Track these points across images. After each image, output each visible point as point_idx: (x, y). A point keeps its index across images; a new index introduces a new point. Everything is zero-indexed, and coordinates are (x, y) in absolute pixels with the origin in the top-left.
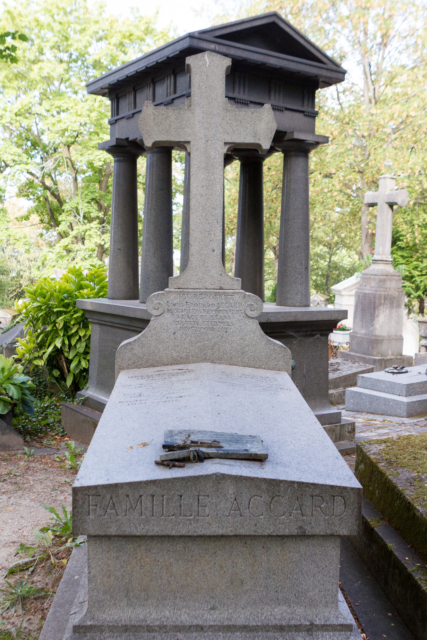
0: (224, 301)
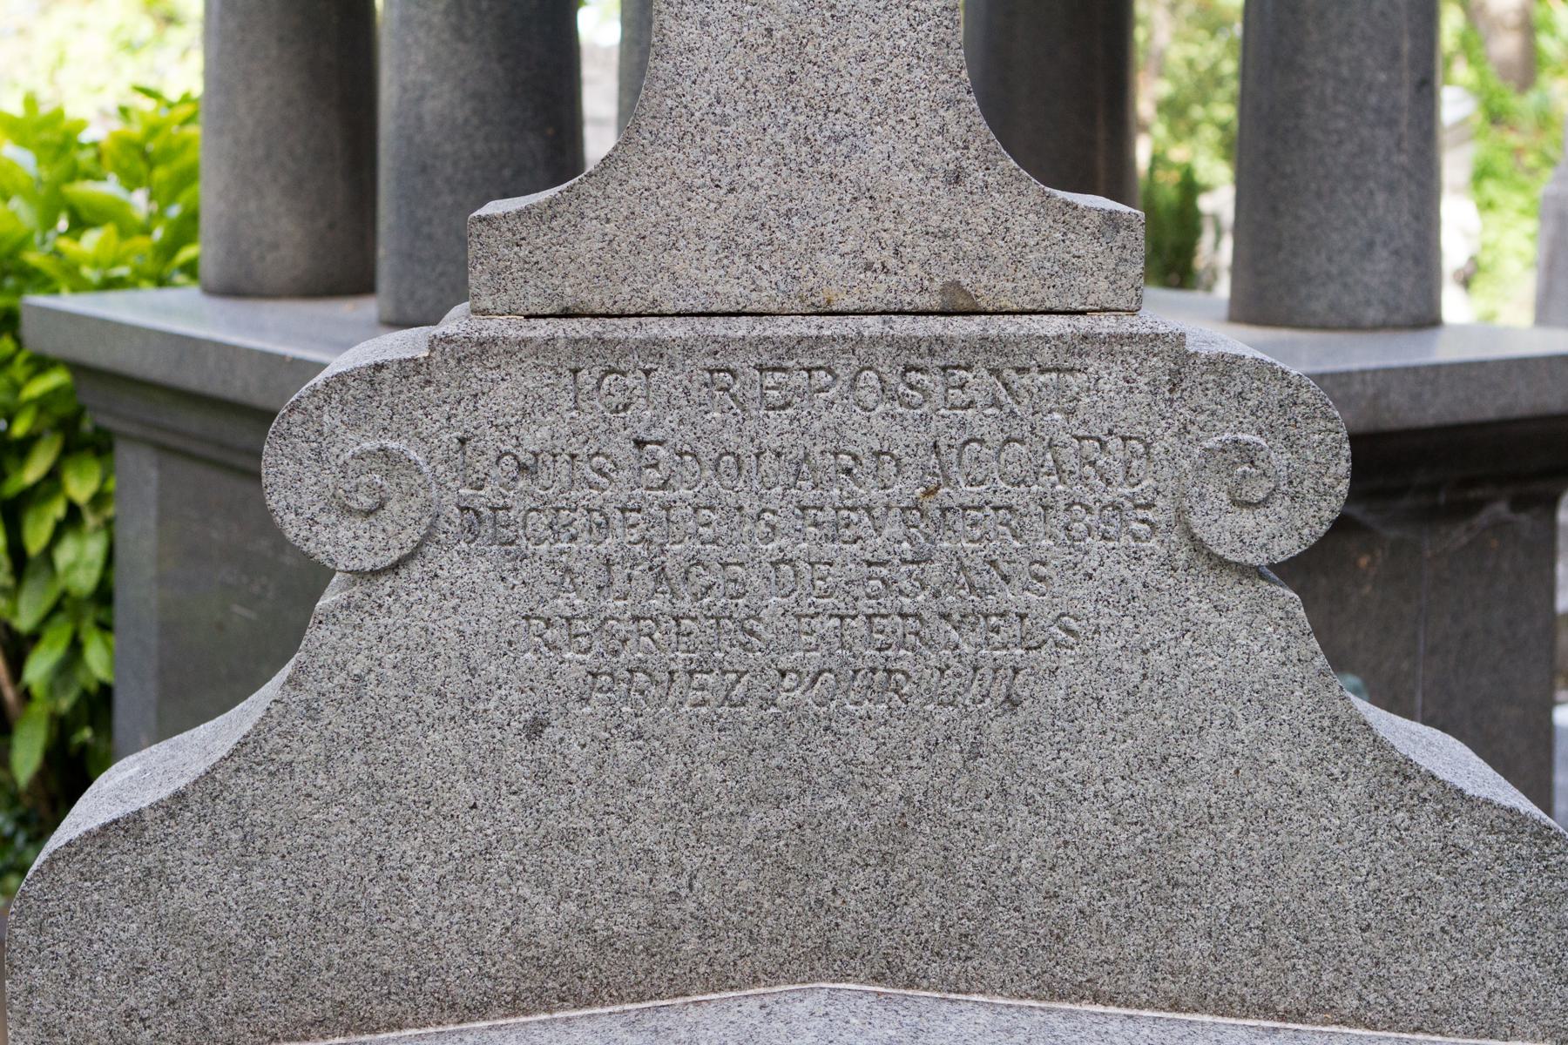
0: (983, 422)
